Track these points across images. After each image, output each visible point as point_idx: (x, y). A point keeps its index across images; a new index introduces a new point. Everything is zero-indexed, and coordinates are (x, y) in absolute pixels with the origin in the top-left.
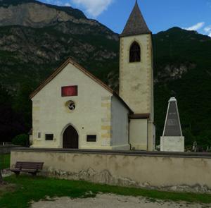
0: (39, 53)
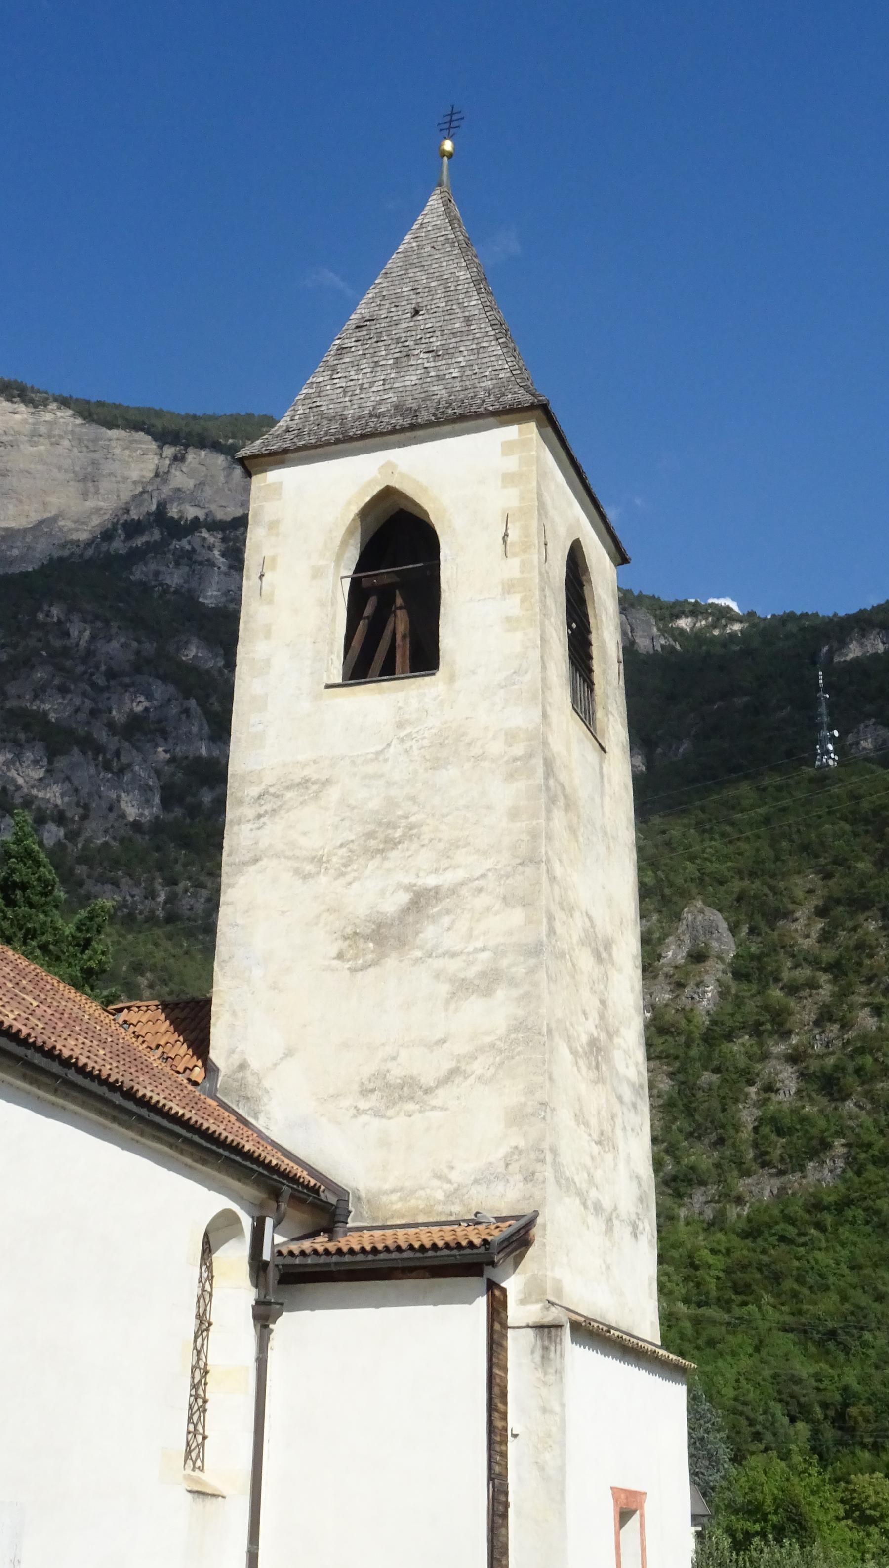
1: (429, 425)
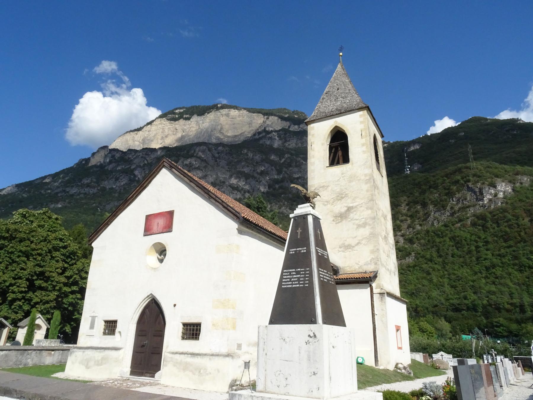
0: (234, 181)
1: (344, 113)
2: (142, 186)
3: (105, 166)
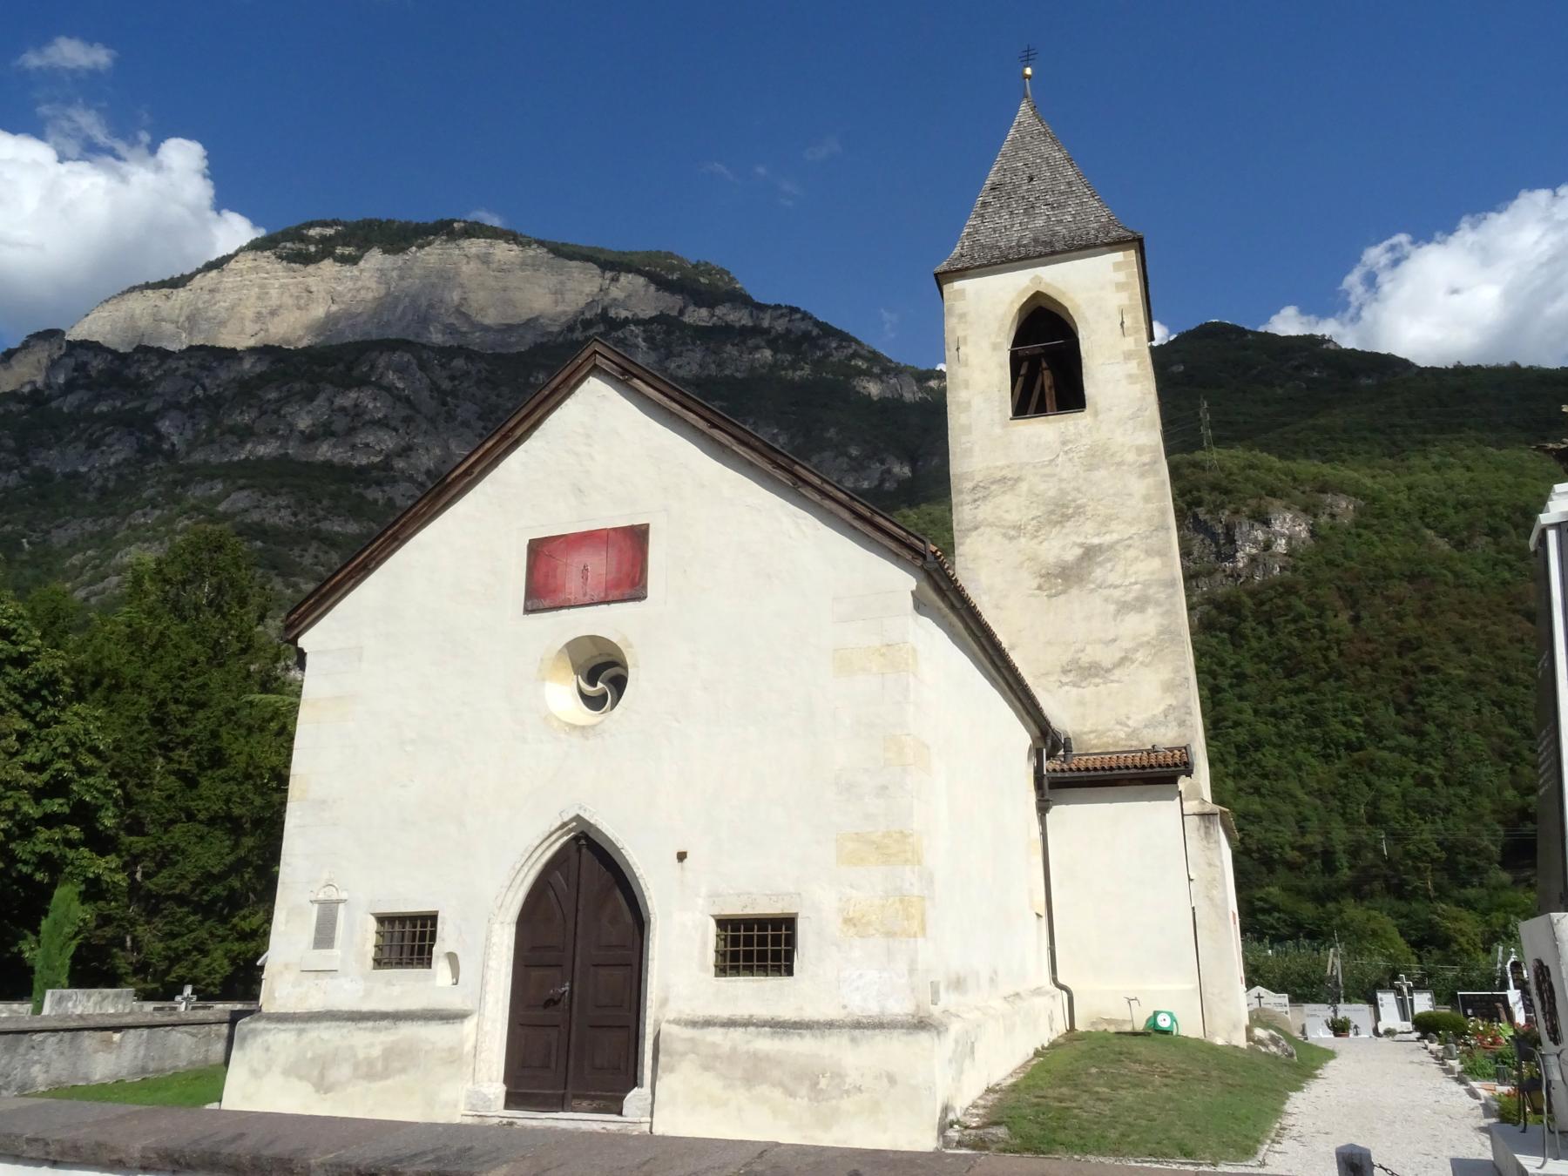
2: (505, 437)
3: (50, 399)
